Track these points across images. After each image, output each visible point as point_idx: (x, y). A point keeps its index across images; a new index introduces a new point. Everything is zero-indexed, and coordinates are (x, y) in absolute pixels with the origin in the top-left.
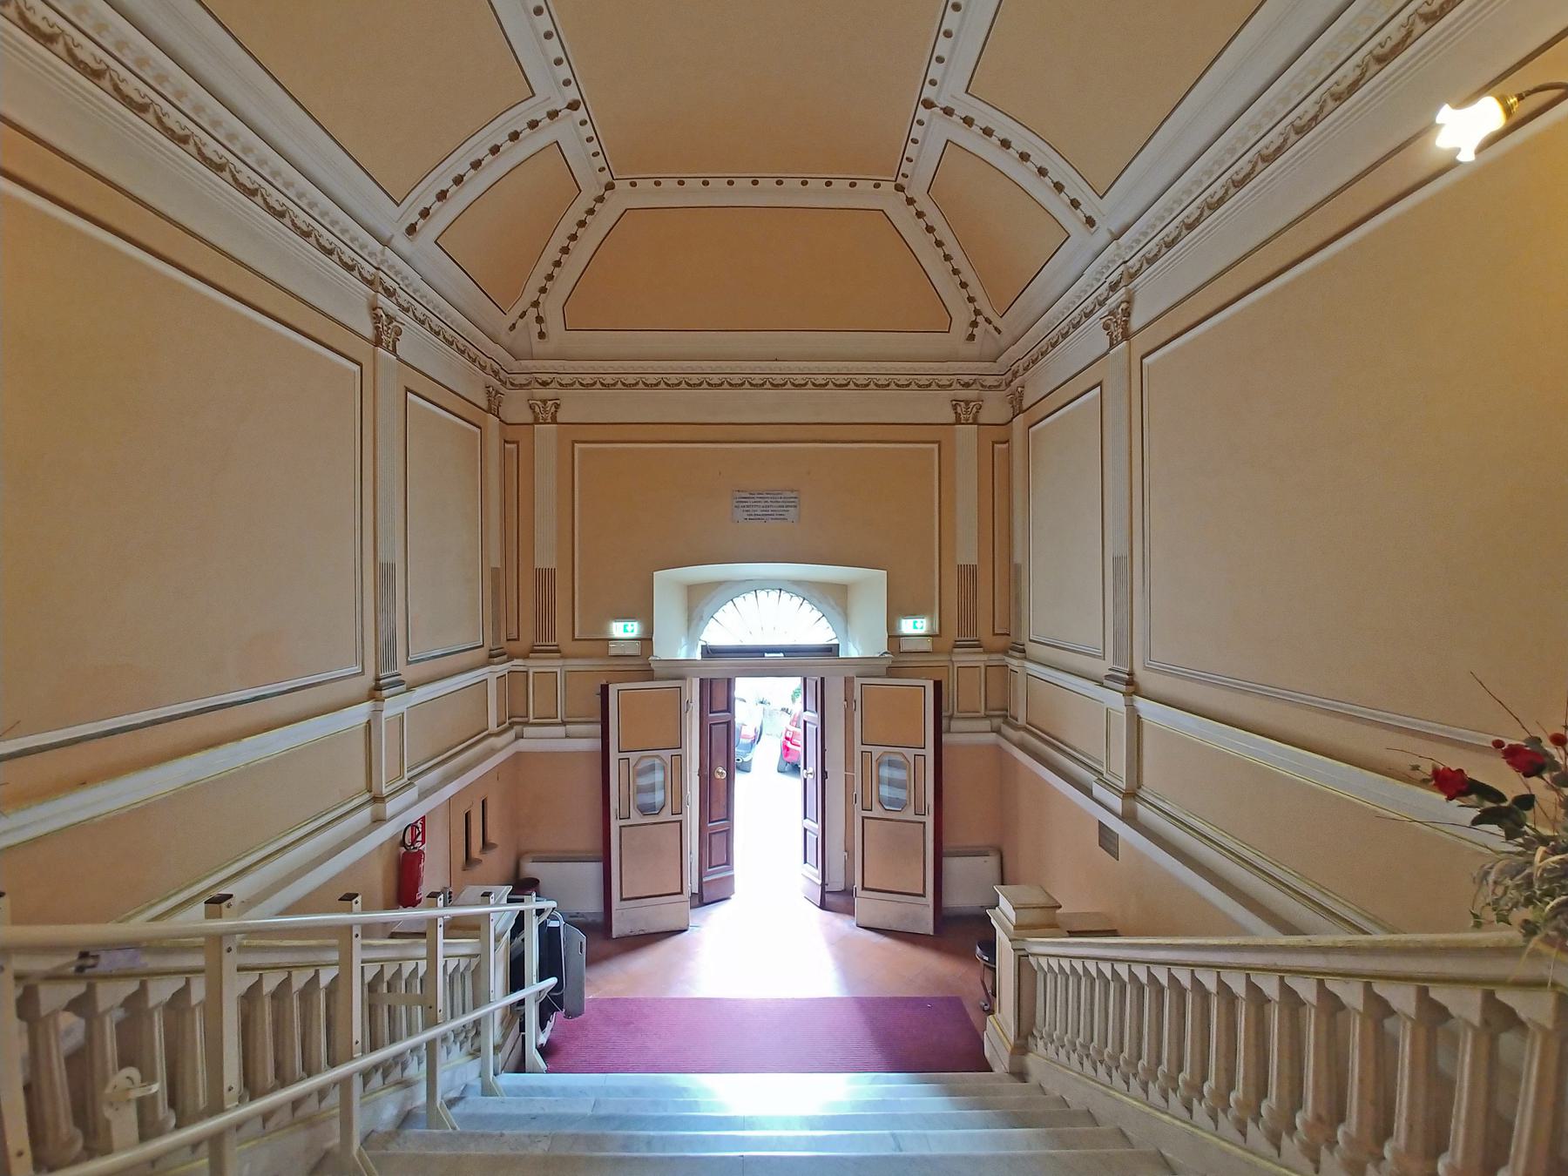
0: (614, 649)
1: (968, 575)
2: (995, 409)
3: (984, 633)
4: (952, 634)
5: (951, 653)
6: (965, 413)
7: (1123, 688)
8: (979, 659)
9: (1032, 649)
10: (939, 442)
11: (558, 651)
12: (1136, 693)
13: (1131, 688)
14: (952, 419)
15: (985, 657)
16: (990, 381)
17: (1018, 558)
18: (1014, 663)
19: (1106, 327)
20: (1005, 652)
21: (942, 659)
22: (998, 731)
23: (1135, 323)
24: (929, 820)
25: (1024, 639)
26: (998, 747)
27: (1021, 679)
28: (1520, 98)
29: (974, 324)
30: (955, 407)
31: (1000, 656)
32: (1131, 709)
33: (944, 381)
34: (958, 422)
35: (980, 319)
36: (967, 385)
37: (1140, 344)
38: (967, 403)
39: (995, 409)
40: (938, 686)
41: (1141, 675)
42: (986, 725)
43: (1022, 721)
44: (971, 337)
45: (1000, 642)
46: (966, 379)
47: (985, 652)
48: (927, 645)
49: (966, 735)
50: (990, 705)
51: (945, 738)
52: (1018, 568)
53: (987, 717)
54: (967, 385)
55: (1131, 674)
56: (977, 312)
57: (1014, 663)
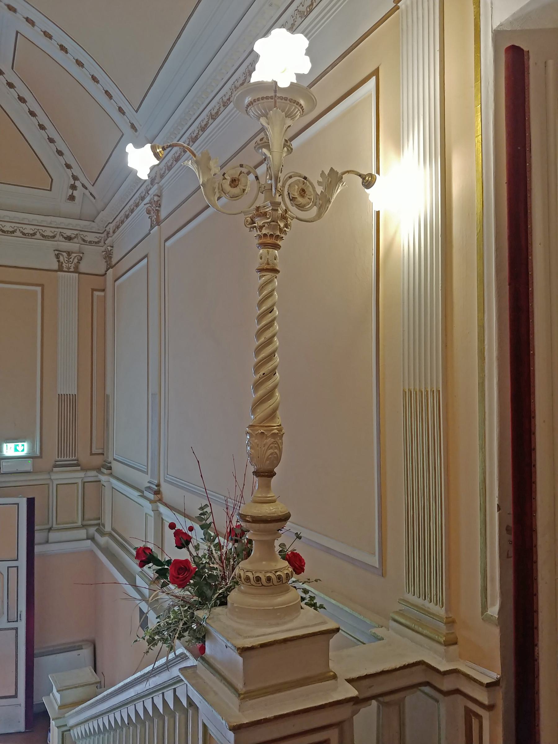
0: (6, 467)
1: (68, 403)
2: (93, 262)
3: (83, 456)
4: (52, 455)
5: (50, 472)
6: (68, 262)
7: (152, 496)
8: (78, 476)
9: (117, 467)
10: (42, 286)
11: (77, 465)
12: (160, 500)
13: (157, 497)
14: (56, 266)
15: (82, 474)
16: (91, 237)
17: (108, 391)
18: (103, 478)
19: (148, 212)
20: (98, 469)
21: (41, 478)
22: (93, 539)
23: (163, 215)
24: (22, 626)
25: (110, 459)
26: (92, 551)
27: (107, 493)
28: (164, 149)
29: (74, 187)
30: (57, 256)
31: (94, 473)
32: (156, 510)
33: (48, 232)
34: (60, 269)
35: (78, 184)
36: (69, 239)
37: (167, 227)
38: (69, 253)
39: (93, 262)
40: (31, 503)
41: (165, 489)
42: (82, 533)
43: (108, 529)
44: (72, 198)
45: (97, 461)
46: (68, 233)
47: (82, 470)
48: (28, 466)
49: (58, 546)
50: (86, 517)
51: (37, 549)
52: (108, 396)
53: (84, 526)
54: (69, 239)
55: (158, 485)
56: (75, 178)
57: (103, 478)
